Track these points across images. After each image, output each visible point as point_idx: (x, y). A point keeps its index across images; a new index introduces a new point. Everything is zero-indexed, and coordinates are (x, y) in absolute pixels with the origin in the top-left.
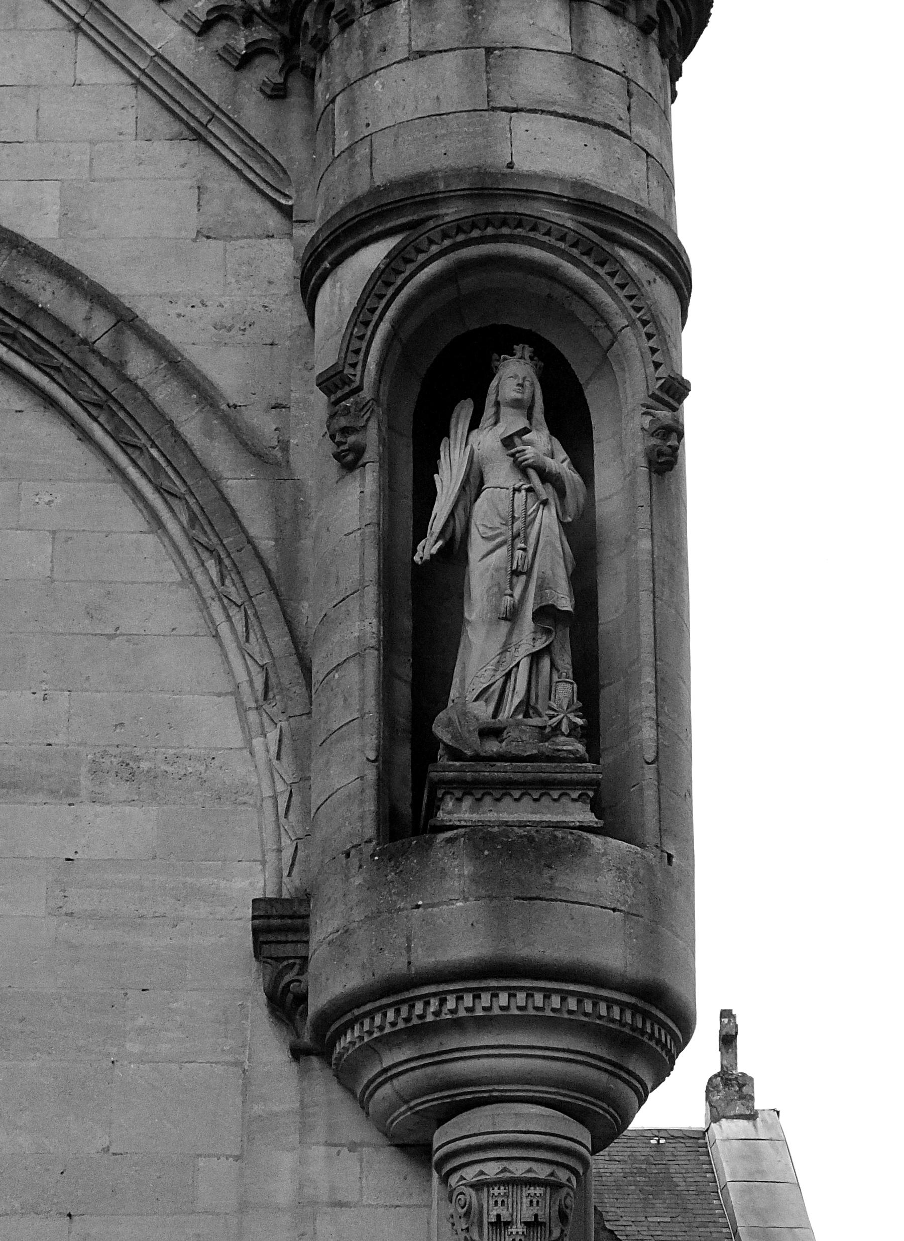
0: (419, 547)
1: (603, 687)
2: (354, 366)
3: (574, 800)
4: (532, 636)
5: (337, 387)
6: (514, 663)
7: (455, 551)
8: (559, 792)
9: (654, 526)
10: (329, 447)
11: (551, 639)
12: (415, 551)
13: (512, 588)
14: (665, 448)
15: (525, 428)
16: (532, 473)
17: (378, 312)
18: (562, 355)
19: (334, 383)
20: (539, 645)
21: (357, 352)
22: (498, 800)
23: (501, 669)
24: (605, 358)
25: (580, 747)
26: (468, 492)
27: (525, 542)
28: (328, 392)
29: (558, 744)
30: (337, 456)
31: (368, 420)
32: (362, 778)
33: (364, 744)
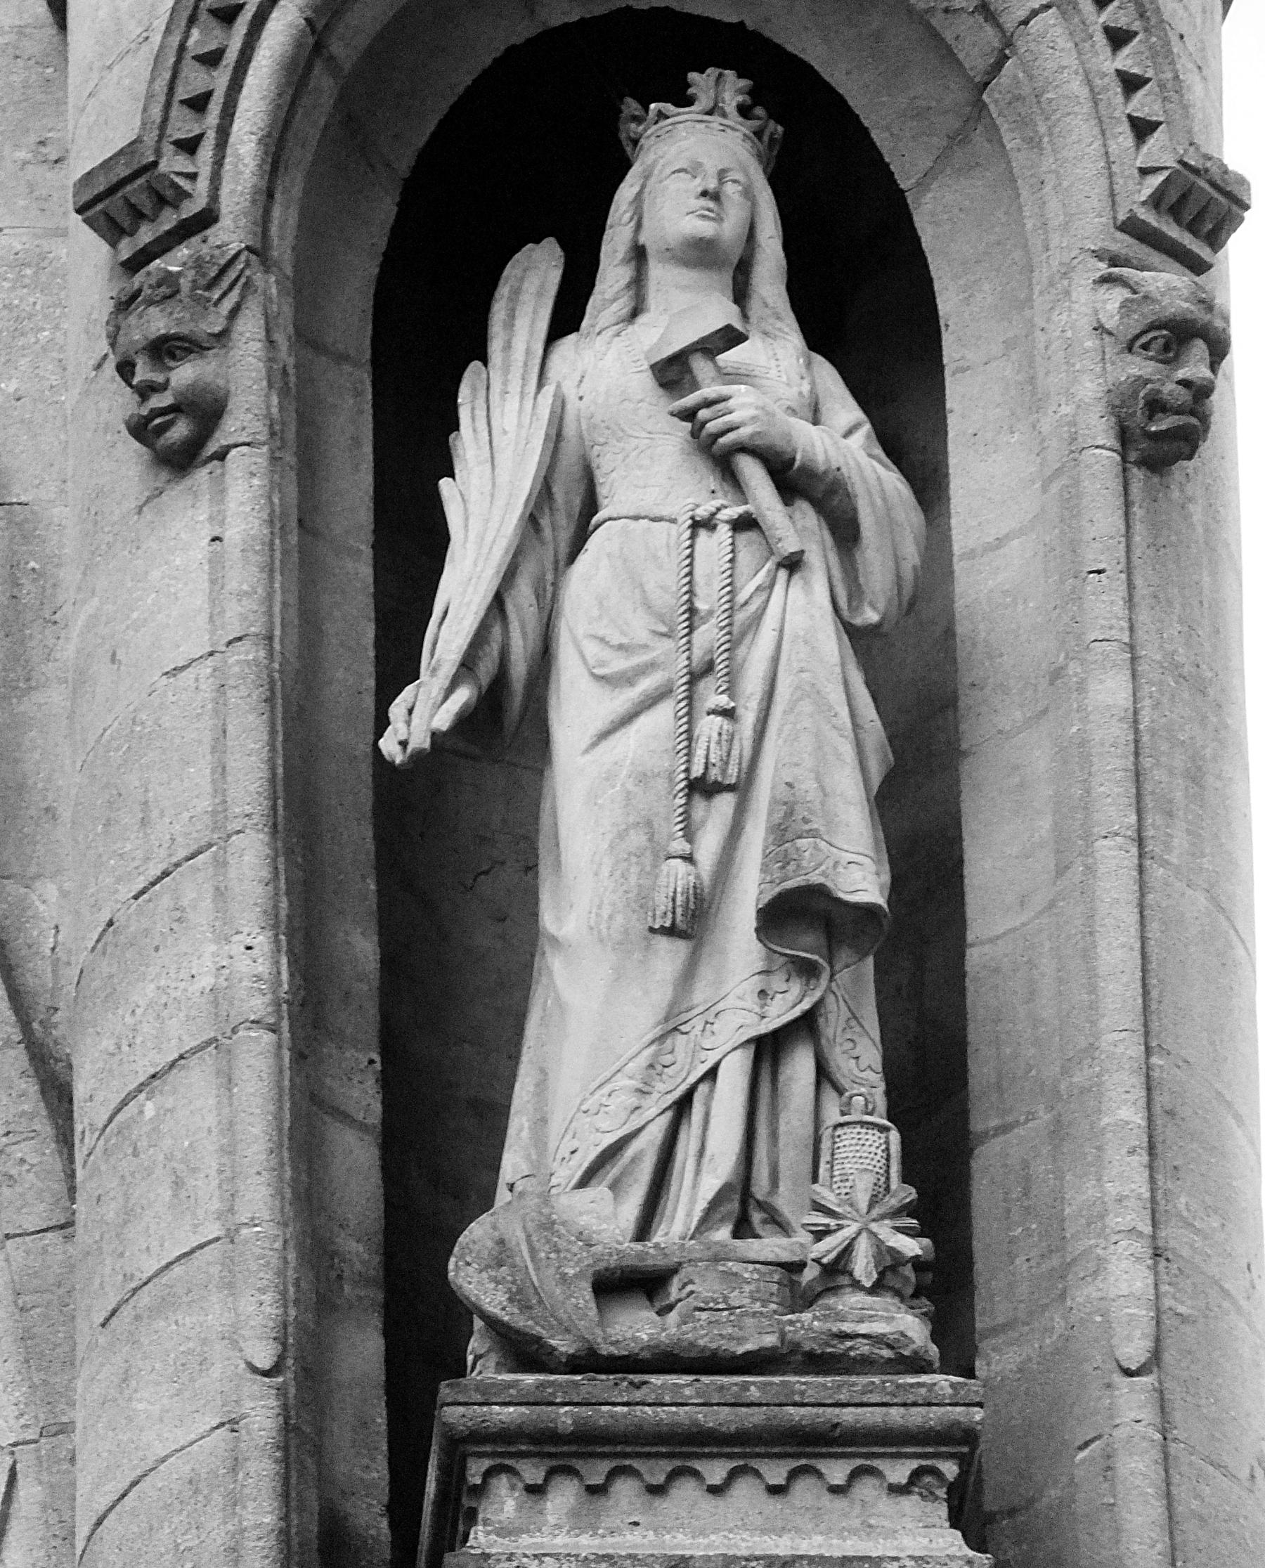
0: (397, 710)
1: (985, 1136)
2: (189, 146)
3: (897, 1490)
4: (756, 983)
5: (139, 215)
6: (701, 1070)
7: (507, 722)
8: (605, 1466)
9: (1141, 634)
10: (119, 403)
11: (817, 994)
12: (382, 723)
13: (689, 834)
14: (1169, 387)
15: (728, 328)
16: (751, 470)
18: (841, 101)
19: (130, 203)
20: (781, 1012)
21: (199, 104)
22: (657, 1491)
23: (660, 1087)
24: (975, 110)
25: (910, 1326)
26: (547, 532)
27: (731, 691)
28: (112, 230)
30: (141, 430)
31: (235, 312)
32: (232, 1424)
33: (244, 1316)
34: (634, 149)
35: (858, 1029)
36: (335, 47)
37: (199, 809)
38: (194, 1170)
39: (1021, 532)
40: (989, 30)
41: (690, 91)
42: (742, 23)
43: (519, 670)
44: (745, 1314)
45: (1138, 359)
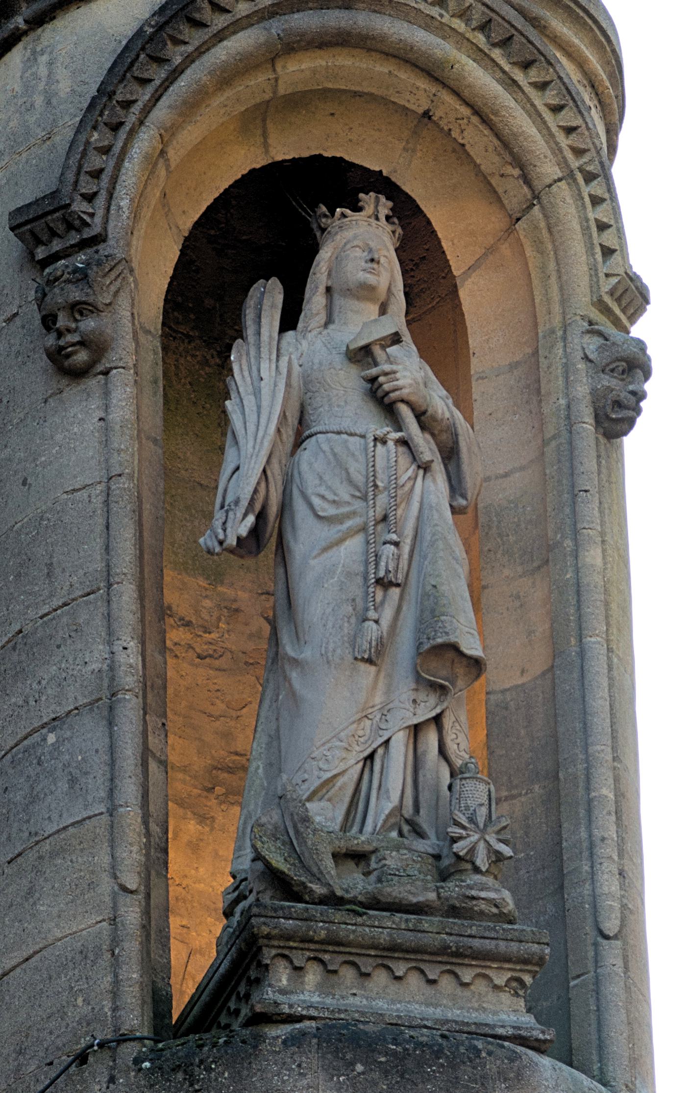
2: (90, 198)
5: (53, 234)
17: (136, 109)
20: (425, 714)
21: (97, 174)
29: (470, 887)
31: (116, 293)
34: (322, 235)
35: (458, 728)
36: (171, 153)
37: (91, 569)
38: (86, 773)
39: (522, 468)
40: (526, 189)
41: (361, 204)
42: (381, 172)
43: (273, 510)
44: (417, 879)
45: (607, 377)
